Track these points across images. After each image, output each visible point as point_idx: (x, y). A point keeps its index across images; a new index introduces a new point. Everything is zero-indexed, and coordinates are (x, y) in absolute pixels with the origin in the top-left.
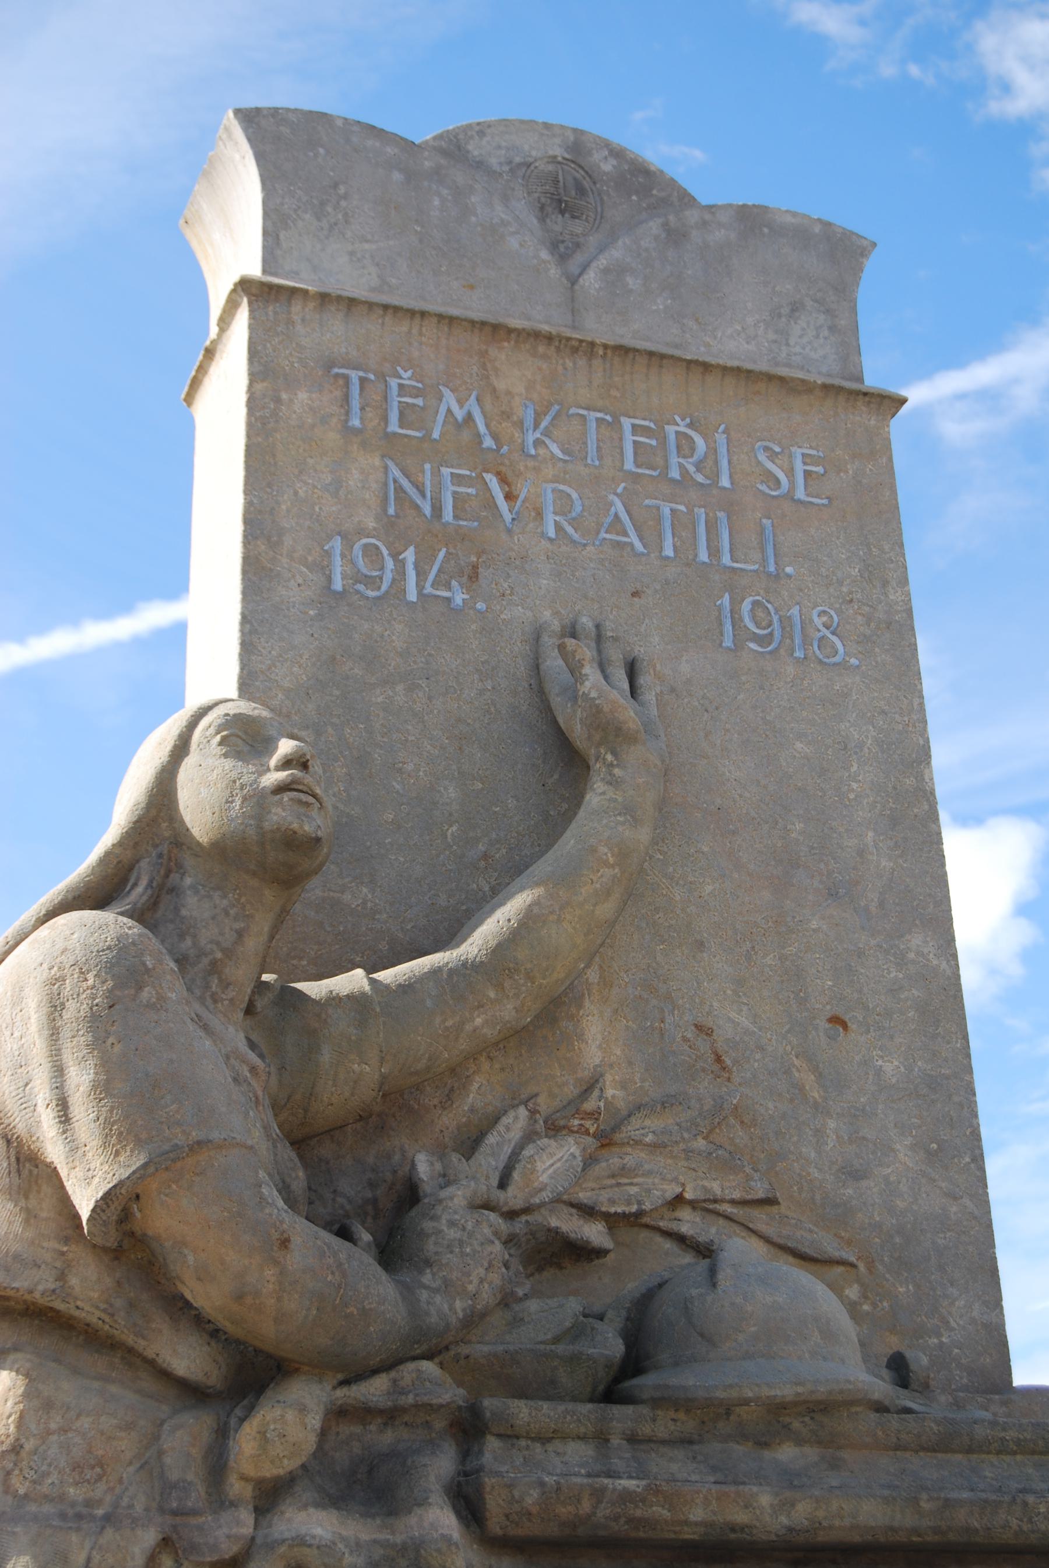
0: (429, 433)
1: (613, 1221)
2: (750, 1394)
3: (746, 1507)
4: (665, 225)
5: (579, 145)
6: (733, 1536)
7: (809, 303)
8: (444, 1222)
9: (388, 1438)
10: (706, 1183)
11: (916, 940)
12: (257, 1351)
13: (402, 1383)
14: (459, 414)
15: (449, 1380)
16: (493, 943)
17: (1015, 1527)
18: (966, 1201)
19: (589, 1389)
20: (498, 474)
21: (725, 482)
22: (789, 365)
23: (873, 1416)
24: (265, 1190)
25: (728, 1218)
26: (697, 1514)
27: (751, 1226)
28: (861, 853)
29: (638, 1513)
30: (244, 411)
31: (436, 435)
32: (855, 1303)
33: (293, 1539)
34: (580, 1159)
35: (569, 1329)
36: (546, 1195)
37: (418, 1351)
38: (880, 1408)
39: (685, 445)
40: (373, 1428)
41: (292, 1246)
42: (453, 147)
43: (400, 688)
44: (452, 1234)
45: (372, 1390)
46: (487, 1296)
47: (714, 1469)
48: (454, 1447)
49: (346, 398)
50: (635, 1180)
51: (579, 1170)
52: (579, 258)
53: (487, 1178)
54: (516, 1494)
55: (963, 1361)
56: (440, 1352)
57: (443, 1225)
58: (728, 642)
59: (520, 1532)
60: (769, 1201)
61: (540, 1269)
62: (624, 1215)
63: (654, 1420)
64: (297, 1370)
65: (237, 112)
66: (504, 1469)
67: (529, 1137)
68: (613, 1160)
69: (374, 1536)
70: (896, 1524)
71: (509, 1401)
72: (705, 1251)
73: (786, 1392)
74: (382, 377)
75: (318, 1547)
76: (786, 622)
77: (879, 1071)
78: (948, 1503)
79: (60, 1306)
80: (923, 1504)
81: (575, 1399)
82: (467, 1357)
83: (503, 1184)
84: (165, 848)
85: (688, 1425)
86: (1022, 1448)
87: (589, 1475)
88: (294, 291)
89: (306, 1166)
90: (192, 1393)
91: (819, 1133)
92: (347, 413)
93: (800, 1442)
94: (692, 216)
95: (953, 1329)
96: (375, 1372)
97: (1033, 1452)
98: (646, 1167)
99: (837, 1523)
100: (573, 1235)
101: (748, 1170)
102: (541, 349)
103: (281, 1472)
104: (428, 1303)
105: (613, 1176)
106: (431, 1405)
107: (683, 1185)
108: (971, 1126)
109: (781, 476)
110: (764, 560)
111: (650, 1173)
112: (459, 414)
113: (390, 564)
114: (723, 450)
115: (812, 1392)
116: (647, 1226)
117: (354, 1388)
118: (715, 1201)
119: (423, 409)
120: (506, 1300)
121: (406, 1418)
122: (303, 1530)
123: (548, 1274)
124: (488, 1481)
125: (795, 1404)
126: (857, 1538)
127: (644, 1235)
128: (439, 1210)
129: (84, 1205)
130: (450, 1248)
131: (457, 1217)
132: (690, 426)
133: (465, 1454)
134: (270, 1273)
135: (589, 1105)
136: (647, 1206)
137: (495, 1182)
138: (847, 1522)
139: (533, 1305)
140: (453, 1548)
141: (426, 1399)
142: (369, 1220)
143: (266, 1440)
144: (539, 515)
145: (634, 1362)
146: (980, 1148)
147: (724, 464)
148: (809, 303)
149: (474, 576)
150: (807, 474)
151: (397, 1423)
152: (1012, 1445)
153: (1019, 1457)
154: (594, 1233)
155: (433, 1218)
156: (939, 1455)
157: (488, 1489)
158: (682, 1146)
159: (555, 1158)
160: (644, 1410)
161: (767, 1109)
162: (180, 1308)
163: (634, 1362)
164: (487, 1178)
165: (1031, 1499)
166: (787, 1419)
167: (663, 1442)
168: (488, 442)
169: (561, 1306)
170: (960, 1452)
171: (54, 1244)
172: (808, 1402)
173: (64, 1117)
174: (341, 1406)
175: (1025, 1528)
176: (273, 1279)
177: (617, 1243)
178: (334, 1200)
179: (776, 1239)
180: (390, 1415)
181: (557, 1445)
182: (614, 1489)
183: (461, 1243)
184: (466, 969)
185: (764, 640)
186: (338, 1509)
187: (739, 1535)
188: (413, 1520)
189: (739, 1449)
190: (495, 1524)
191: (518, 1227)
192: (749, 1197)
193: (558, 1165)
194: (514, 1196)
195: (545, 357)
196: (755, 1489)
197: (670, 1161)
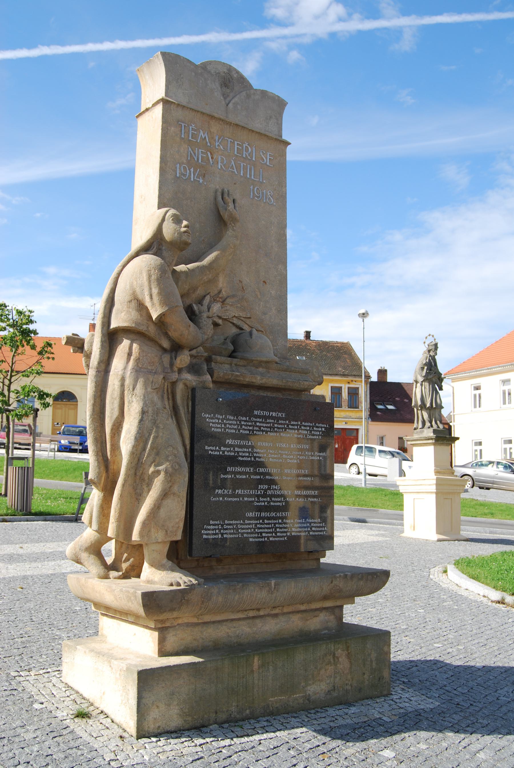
0: (197, 141)
1: (223, 319)
4: (247, 93)
5: (230, 69)
7: (273, 117)
11: (280, 266)
14: (203, 137)
16: (209, 262)
20: (210, 152)
21: (254, 159)
22: (268, 131)
25: (242, 320)
26: (247, 380)
28: (272, 247)
30: (161, 131)
31: (198, 141)
38: (277, 363)
39: (247, 150)
42: (204, 66)
43: (189, 201)
44: (205, 323)
47: (250, 372)
49: (181, 130)
52: (228, 99)
58: (251, 197)
65: (161, 52)
74: (189, 126)
76: (263, 193)
77: (271, 293)
79: (147, 333)
81: (225, 356)
84: (159, 240)
86: (299, 372)
88: (172, 102)
90: (165, 350)
91: (259, 305)
92: (181, 134)
93: (263, 368)
94: (252, 92)
102: (220, 122)
109: (265, 159)
110: (260, 179)
112: (203, 137)
113: (188, 172)
114: (254, 151)
119: (196, 134)
127: (227, 322)
129: (154, 316)
132: (248, 145)
135: (220, 296)
144: (218, 163)
147: (254, 154)
148: (273, 117)
149: (204, 176)
150: (270, 159)
160: (239, 360)
162: (166, 335)
168: (209, 144)
171: (145, 321)
173: (151, 297)
184: (203, 267)
185: (258, 197)
188: (204, 377)
189: (253, 368)
195: (221, 124)
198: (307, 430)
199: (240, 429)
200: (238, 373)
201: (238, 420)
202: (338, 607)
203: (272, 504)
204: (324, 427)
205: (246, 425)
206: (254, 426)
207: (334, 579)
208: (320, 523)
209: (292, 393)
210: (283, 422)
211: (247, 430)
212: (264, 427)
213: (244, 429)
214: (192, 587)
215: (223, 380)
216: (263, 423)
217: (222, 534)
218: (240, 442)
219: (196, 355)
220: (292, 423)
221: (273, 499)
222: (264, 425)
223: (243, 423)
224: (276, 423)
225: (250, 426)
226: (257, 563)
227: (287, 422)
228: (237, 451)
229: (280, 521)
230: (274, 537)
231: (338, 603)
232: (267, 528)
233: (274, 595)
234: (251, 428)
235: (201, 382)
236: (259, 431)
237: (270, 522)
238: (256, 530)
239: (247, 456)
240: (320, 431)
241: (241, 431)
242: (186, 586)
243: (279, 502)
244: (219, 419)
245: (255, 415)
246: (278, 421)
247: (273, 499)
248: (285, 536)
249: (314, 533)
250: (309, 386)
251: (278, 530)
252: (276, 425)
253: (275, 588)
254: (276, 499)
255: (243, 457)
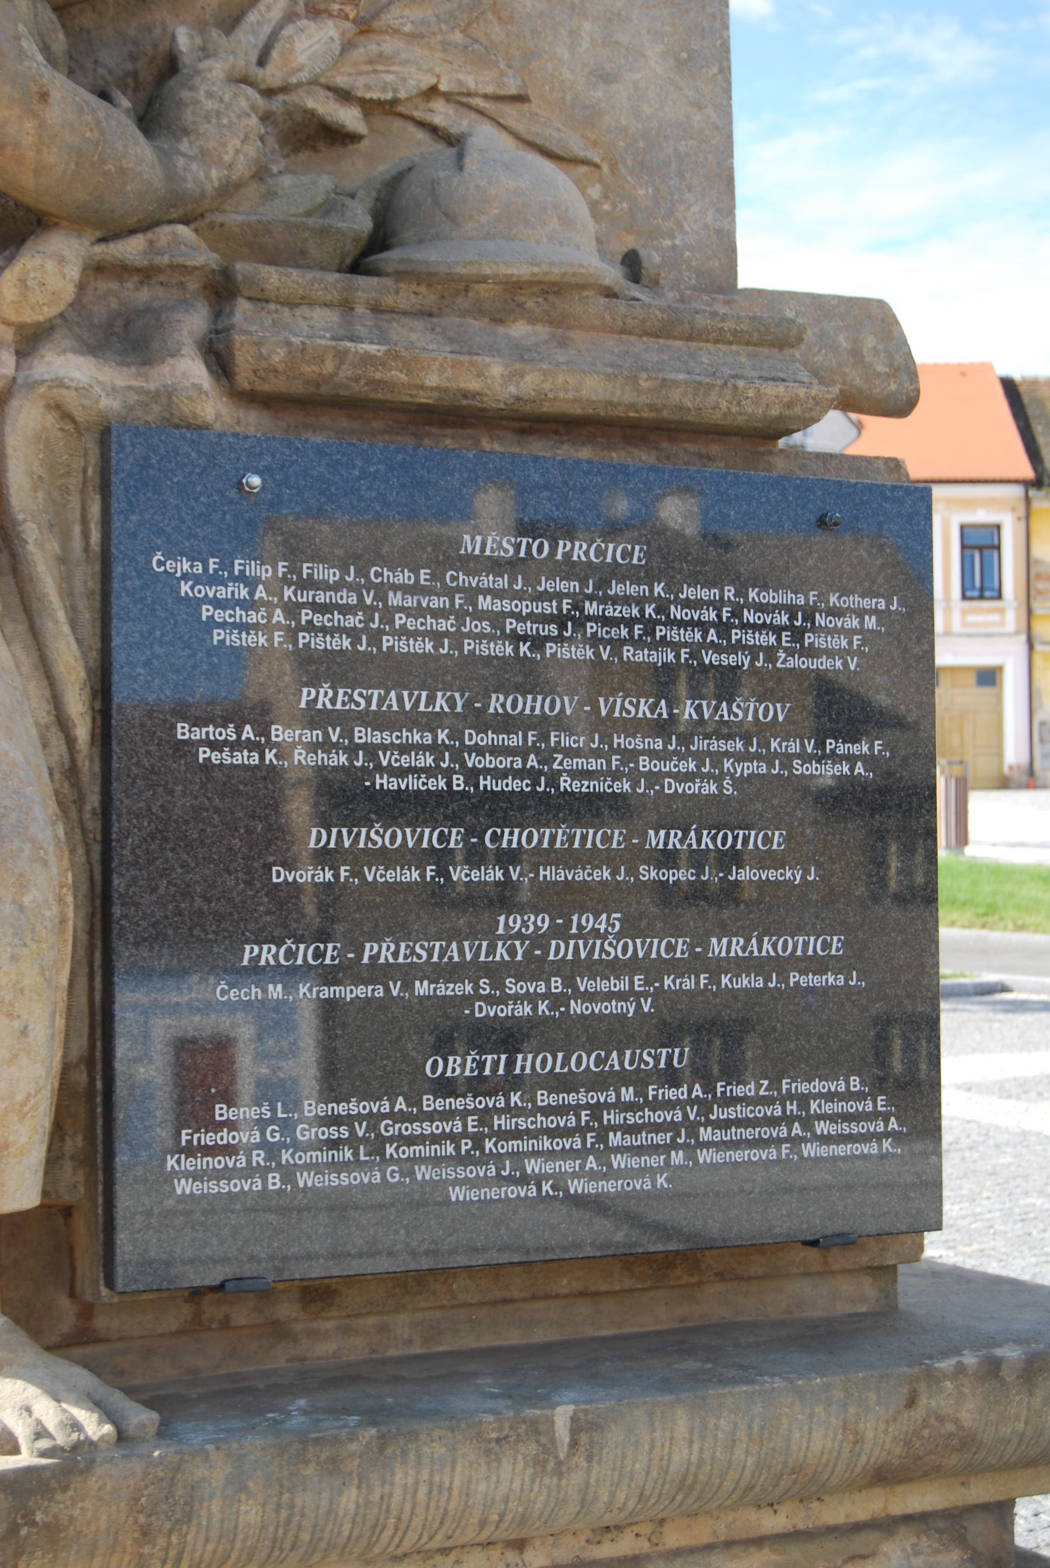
1: (369, 107)
2: (489, 272)
3: (478, 376)
6: (465, 402)
8: (202, 92)
9: (143, 296)
10: (461, 77)
12: (18, 205)
13: (159, 245)
15: (204, 245)
17: (724, 409)
18: (710, 111)
19: (337, 261)
23: (602, 300)
24: (24, 43)
25: (480, 112)
26: (432, 380)
27: (502, 121)
29: (378, 376)
32: (596, 202)
33: (52, 380)
34: (338, 42)
35: (320, 205)
36: (304, 76)
37: (174, 216)
38: (610, 294)
40: (129, 285)
41: (51, 100)
44: (210, 105)
45: (129, 249)
46: (242, 168)
47: (451, 340)
48: (207, 307)
50: (392, 69)
51: (337, 53)
53: (246, 54)
54: (264, 351)
55: (693, 263)
56: (196, 219)
57: (201, 96)
59: (266, 388)
60: (521, 98)
61: (296, 151)
62: (380, 103)
63: (397, 292)
64: (56, 225)
66: (253, 329)
67: (289, 17)
68: (371, 47)
69: (128, 383)
70: (615, 400)
71: (260, 267)
72: (454, 141)
73: (522, 271)
75: (76, 390)
78: (664, 383)
80: (641, 382)
82: (222, 225)
83: (262, 61)
85: (429, 298)
86: (737, 338)
87: (333, 338)
89: (68, 34)
93: (532, 320)
95: (686, 233)
96: (132, 232)
97: (748, 343)
98: (403, 56)
99: (561, 395)
100: (328, 118)
101: (502, 66)
103: (41, 318)
104: (185, 169)
105: (370, 62)
106: (185, 267)
107: (438, 76)
108: (722, 37)
111: (405, 62)
115: (547, 273)
116: (401, 115)
117: (112, 245)
118: (469, 94)
120: (261, 174)
121: (162, 278)
122: (62, 374)
123: (304, 156)
124: (238, 338)
125: (530, 283)
126: (579, 411)
127: (398, 123)
128: (197, 81)
130: (207, 118)
131: (215, 89)
133: (217, 315)
134: (29, 125)
136: (402, 95)
137: (254, 58)
138: (571, 395)
139: (287, 180)
140: (204, 397)
141: (181, 260)
142: (130, 92)
143: (27, 287)
145: (380, 240)
146: (728, 60)
151: (153, 282)
152: (728, 335)
153: (734, 347)
154: (349, 117)
155: (192, 88)
156: (661, 341)
157: (237, 346)
158: (439, 37)
159: (314, 40)
160: (388, 282)
161: (525, 7)
163: (380, 240)
164: (246, 54)
165: (741, 384)
166: (523, 299)
167: (405, 313)
169: (314, 183)
170: (681, 339)
172: (543, 283)
174: (99, 262)
175: (733, 410)
176: (32, 132)
177: (372, 131)
178: (95, 70)
179: (525, 135)
180: (146, 274)
181: (305, 310)
182: (356, 352)
183: (218, 114)
186: (95, 357)
187: (470, 402)
188: (165, 369)
189: (475, 324)
190: (244, 380)
191: (276, 104)
192: (502, 93)
193: (317, 46)
194: (272, 74)
196: (487, 360)
197: (426, 52)
198: (778, 630)
199: (381, 632)
200: (372, 348)
201: (369, 586)
202: (985, 1507)
203: (576, 1007)
204: (875, 612)
205: (419, 612)
206: (461, 616)
207: (922, 1387)
208: (860, 1096)
209: (715, 449)
210: (632, 590)
211: (424, 634)
212: (519, 617)
213: (404, 632)
214: (74, 1460)
215: (297, 388)
216: (519, 596)
217: (288, 1174)
218: (381, 700)
219: (141, 261)
220: (688, 592)
221: (584, 984)
222: (525, 607)
223: (395, 599)
224: (591, 598)
225: (437, 614)
226: (534, 1298)
227: (658, 589)
228: (365, 747)
229: (628, 1094)
230: (593, 1176)
231: (979, 1492)
232: (553, 1133)
233: (576, 1478)
234: (445, 625)
235: (156, 396)
236: (491, 638)
237: (571, 1099)
238: (489, 1145)
239: (425, 770)
240: (849, 633)
241: (387, 642)
242: (43, 1454)
243: (621, 996)
244: (252, 583)
245: (470, 557)
246: (603, 584)
247: (584, 984)
248: (660, 1170)
249: (823, 1151)
250: (790, 405)
251: (615, 1139)
252: (591, 608)
253: (574, 1444)
254: (602, 985)
255: (402, 773)
